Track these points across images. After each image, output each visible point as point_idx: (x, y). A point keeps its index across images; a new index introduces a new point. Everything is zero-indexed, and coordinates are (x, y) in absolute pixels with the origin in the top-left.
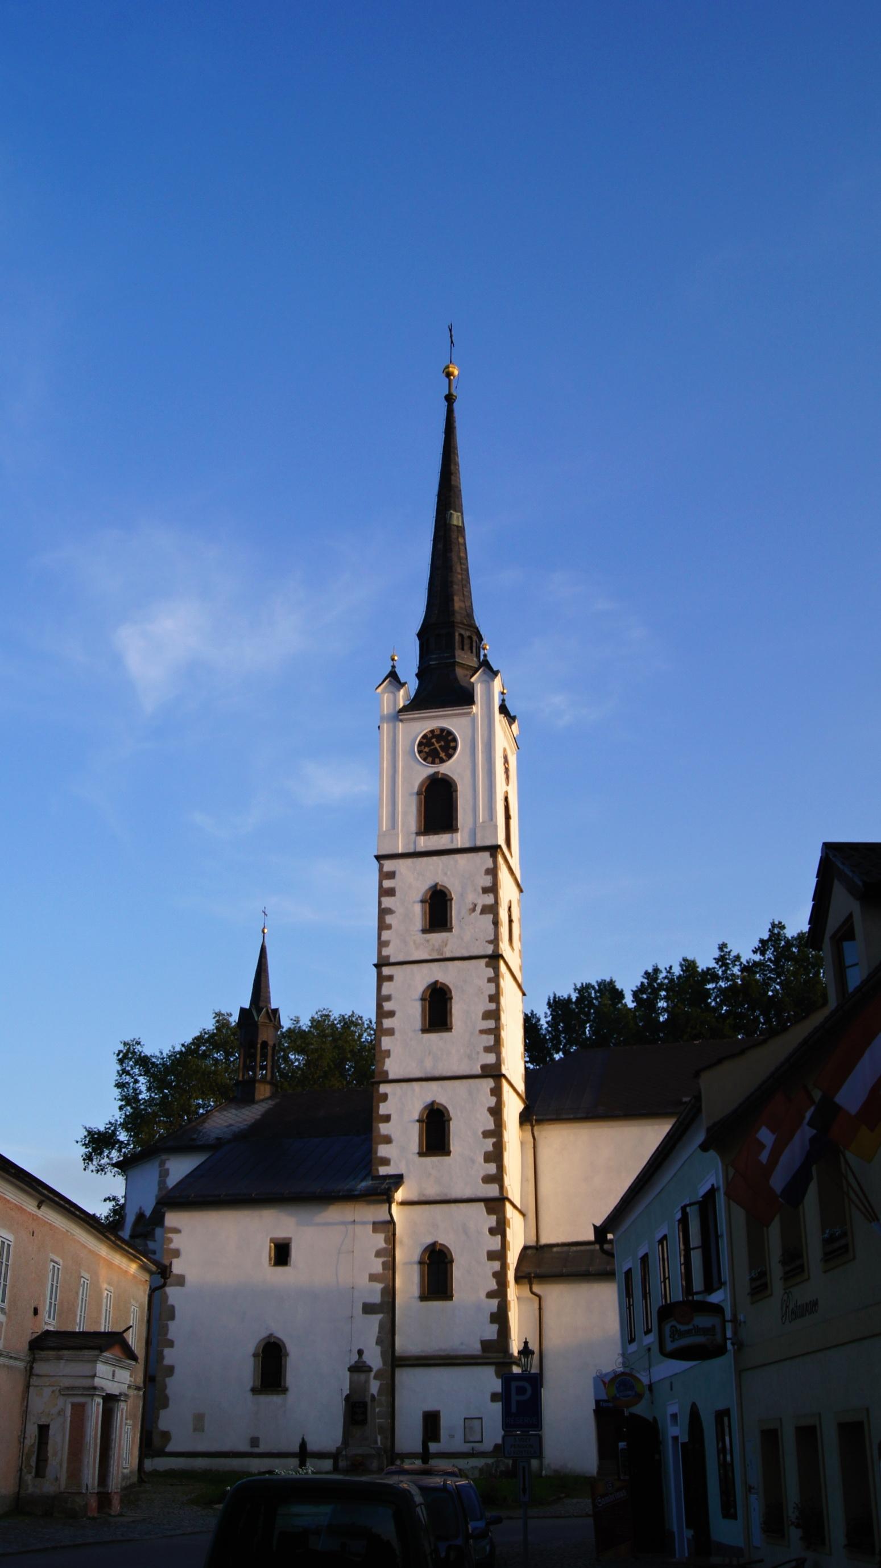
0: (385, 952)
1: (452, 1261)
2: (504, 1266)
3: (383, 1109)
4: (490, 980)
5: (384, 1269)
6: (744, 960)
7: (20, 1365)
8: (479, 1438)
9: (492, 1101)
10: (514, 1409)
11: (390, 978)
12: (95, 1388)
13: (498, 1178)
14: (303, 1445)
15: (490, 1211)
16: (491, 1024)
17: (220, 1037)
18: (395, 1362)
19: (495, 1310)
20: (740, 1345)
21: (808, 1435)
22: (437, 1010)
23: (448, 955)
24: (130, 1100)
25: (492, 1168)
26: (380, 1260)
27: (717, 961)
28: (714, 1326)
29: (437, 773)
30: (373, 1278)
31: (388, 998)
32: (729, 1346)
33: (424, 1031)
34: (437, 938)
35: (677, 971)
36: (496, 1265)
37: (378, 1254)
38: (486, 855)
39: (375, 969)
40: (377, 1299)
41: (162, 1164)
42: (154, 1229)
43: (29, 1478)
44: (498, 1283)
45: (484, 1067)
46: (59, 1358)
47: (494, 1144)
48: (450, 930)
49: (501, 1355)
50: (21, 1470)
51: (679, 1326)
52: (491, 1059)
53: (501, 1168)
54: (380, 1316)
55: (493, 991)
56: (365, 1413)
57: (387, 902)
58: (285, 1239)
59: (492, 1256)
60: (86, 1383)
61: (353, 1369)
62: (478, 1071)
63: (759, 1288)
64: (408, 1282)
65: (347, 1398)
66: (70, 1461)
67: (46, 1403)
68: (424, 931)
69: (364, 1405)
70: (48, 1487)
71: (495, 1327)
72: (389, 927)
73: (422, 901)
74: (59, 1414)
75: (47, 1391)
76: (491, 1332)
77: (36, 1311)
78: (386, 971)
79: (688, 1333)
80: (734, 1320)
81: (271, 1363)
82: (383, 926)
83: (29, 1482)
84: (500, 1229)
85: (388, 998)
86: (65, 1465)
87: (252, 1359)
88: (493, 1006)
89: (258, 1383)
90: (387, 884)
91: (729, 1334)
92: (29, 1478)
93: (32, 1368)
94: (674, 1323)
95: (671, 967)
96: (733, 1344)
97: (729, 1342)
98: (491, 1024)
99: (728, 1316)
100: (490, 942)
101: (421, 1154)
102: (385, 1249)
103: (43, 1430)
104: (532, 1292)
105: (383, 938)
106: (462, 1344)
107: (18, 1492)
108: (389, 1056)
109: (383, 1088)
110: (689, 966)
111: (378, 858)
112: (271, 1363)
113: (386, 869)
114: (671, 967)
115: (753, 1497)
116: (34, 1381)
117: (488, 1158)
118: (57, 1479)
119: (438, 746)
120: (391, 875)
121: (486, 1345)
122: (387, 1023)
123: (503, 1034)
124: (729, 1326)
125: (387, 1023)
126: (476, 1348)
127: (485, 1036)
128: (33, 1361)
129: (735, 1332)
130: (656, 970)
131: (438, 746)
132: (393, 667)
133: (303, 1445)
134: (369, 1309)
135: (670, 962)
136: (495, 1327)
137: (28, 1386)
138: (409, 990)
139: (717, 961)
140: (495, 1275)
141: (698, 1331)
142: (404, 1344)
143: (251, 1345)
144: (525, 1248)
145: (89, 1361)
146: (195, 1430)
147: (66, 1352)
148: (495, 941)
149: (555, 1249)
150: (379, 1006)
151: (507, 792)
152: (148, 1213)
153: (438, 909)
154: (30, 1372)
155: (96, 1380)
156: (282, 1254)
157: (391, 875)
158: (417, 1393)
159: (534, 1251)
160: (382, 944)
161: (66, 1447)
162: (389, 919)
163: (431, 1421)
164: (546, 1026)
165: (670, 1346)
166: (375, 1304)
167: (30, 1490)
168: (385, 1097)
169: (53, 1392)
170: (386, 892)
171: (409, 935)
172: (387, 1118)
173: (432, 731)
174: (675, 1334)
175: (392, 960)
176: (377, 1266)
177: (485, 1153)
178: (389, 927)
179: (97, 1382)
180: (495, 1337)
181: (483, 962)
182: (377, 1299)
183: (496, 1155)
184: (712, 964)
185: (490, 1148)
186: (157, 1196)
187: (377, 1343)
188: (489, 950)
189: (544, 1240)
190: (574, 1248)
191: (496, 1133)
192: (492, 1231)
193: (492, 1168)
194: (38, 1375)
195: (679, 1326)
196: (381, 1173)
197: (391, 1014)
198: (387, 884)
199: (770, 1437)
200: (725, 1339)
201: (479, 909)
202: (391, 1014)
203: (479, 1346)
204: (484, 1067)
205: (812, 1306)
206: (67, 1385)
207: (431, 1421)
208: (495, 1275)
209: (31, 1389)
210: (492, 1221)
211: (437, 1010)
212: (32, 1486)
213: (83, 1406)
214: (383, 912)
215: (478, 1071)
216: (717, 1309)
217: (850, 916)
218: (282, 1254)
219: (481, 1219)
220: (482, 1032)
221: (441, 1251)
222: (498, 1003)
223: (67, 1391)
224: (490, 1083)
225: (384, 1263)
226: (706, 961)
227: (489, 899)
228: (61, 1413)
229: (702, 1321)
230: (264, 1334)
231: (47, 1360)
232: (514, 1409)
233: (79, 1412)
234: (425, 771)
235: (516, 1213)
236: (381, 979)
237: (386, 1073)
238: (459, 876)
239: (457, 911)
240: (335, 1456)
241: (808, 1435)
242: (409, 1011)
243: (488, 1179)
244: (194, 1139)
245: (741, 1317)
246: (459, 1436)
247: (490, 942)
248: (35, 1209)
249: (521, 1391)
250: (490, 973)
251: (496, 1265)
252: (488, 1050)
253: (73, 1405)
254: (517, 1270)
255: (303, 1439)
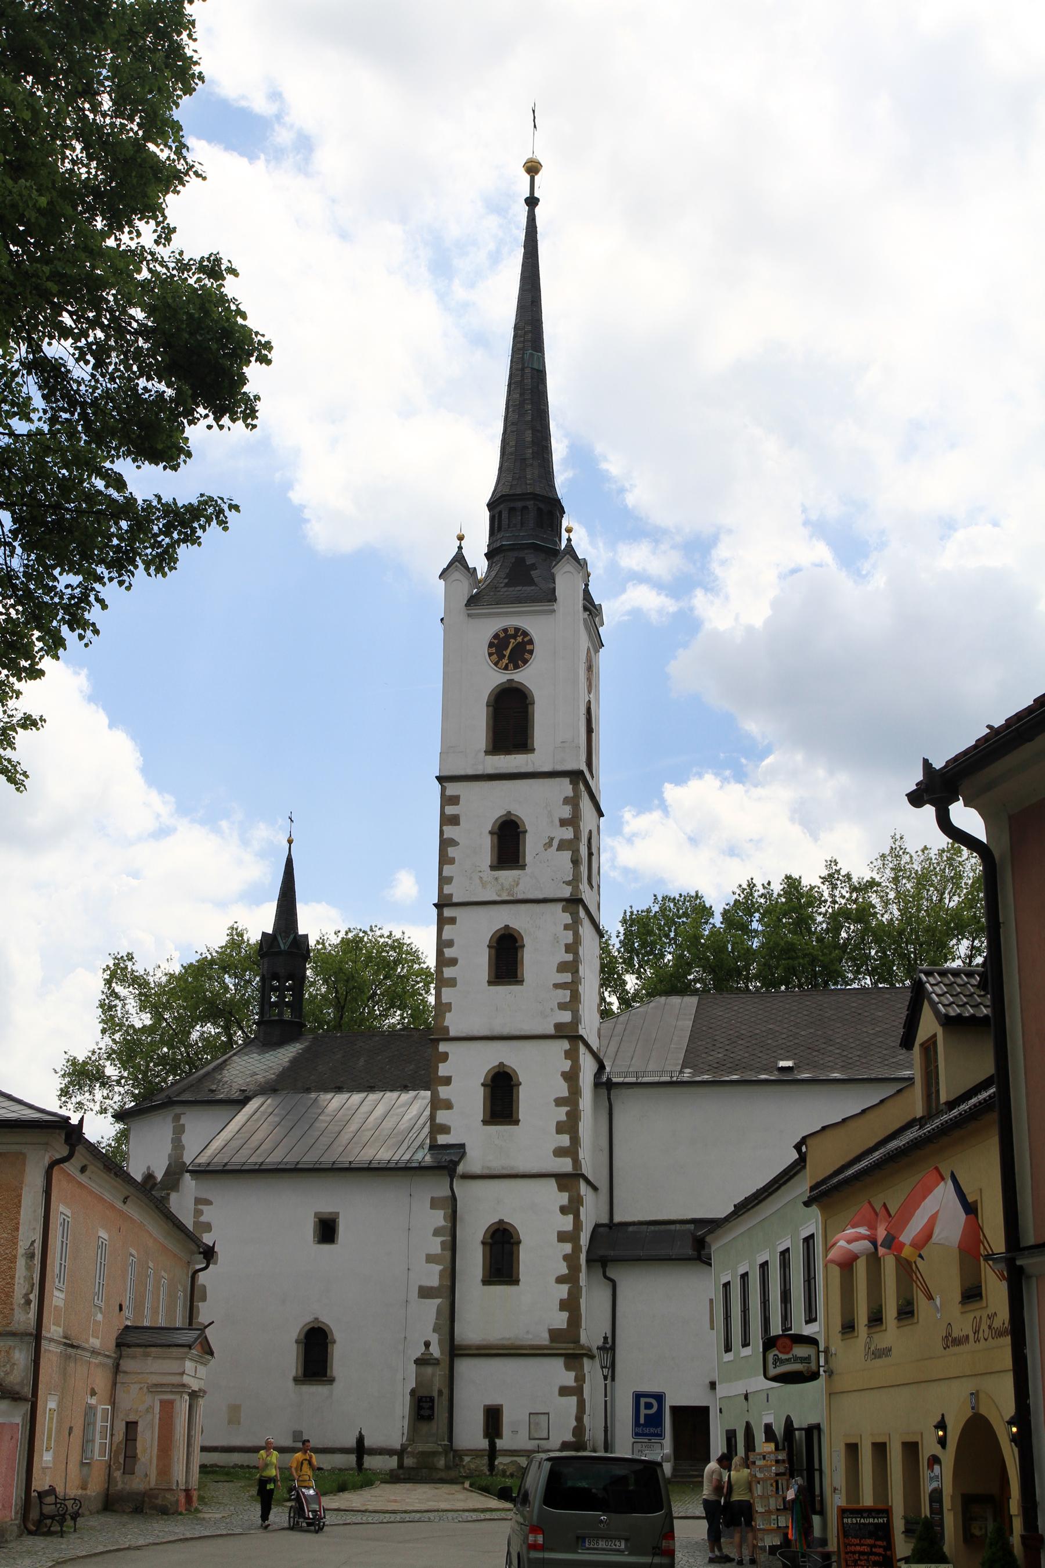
0: (447, 890)
1: (519, 1242)
2: (577, 1248)
3: (443, 1070)
4: (567, 927)
5: (442, 1249)
6: (855, 880)
7: (110, 1361)
8: (545, 1436)
9: (567, 1065)
10: (642, 1421)
11: (452, 921)
12: (184, 1385)
13: (571, 1152)
14: (360, 1440)
15: (561, 1188)
16: (567, 977)
17: (232, 957)
18: (455, 1351)
19: (565, 1296)
20: (830, 1373)
21: (880, 1449)
22: (506, 958)
23: (521, 896)
24: (111, 1022)
25: (565, 1140)
26: (439, 1239)
27: (824, 880)
28: (810, 1356)
29: (510, 681)
30: (430, 1259)
31: (450, 944)
32: (822, 1372)
33: (490, 983)
34: (507, 876)
35: (777, 888)
36: (568, 1248)
37: (437, 1232)
38: (566, 782)
39: (435, 911)
40: (434, 1281)
41: (177, 1118)
42: (168, 1194)
43: (118, 1474)
44: (569, 1267)
45: (558, 1026)
46: (147, 1355)
47: (568, 1114)
48: (523, 867)
49: (572, 1345)
50: (110, 1466)
51: (781, 1356)
52: (566, 1017)
53: (575, 1140)
54: (439, 1301)
55: (570, 940)
56: (432, 1408)
57: (450, 832)
58: (331, 1213)
59: (562, 1237)
60: (175, 1380)
61: (419, 1362)
62: (551, 1031)
63: (848, 1327)
64: (473, 1260)
65: (413, 1392)
66: (159, 1458)
67: (136, 1400)
68: (493, 868)
69: (431, 1399)
70: (137, 1484)
71: (565, 1315)
72: (452, 861)
73: (491, 833)
74: (147, 1411)
75: (134, 1388)
76: (560, 1320)
77: (121, 1309)
78: (448, 912)
79: (788, 1360)
80: (827, 1351)
81: (315, 1352)
82: (444, 859)
83: (118, 1479)
84: (572, 1208)
85: (450, 944)
86: (155, 1461)
87: (295, 1346)
88: (569, 957)
89: (300, 1372)
90: (450, 810)
91: (822, 1363)
92: (118, 1474)
93: (118, 1365)
94: (777, 1352)
95: (769, 883)
96: (825, 1371)
97: (822, 1369)
98: (567, 977)
99: (822, 1348)
100: (568, 883)
101: (485, 1122)
102: (443, 1227)
103: (131, 1427)
104: (605, 1277)
105: (445, 874)
106: (528, 1332)
107: (108, 1489)
108: (450, 1011)
109: (443, 1047)
110: (792, 884)
111: (440, 779)
112: (315, 1352)
113: (448, 793)
114: (769, 883)
115: (837, 1496)
116: (120, 1378)
117: (560, 1128)
118: (146, 1475)
119: (512, 649)
120: (454, 800)
121: (555, 1335)
122: (448, 972)
123: (581, 989)
124: (822, 1355)
125: (448, 972)
126: (544, 1339)
127: (560, 992)
128: (120, 1357)
129: (827, 1362)
130: (751, 885)
131: (512, 649)
132: (460, 548)
133: (360, 1440)
134: (425, 1293)
135: (769, 874)
136: (565, 1315)
137: (114, 1384)
138: (476, 932)
139: (824, 880)
140: (566, 1258)
141: (797, 1359)
142: (468, 1332)
143: (294, 1331)
144: (597, 1226)
145: (176, 1358)
146: (230, 1422)
147: (153, 1349)
148: (575, 882)
149: (631, 1229)
150: (440, 953)
151: (589, 702)
152: (159, 1175)
153: (509, 842)
154: (117, 1369)
155: (185, 1376)
156: (327, 1230)
157: (454, 800)
158: (478, 1385)
159: (607, 1229)
160: (444, 880)
161: (156, 1443)
162: (452, 852)
163: (493, 1417)
164: (618, 945)
165: (773, 1372)
166: (432, 1288)
167: (120, 1486)
168: (445, 1057)
169: (141, 1388)
170: (448, 820)
171: (476, 874)
172: (447, 1081)
173: (505, 630)
174: (777, 1361)
175: (455, 900)
176: (436, 1246)
177: (558, 1123)
178: (452, 861)
179: (186, 1379)
180: (565, 1327)
181: (559, 906)
182: (434, 1281)
183: (570, 1126)
184: (817, 882)
185: (564, 1118)
186: (170, 1156)
187: (434, 1331)
188: (566, 892)
189: (617, 1219)
190: (652, 1228)
191: (571, 1101)
192: (564, 1210)
193: (565, 1140)
194: (125, 1372)
195: (781, 1356)
196: (439, 1142)
197: (453, 962)
198: (450, 810)
199: (852, 1449)
200: (819, 1366)
201: (555, 843)
202: (453, 962)
203: (546, 1335)
204: (558, 1026)
205: (886, 1352)
206: (154, 1382)
207: (493, 1417)
208: (566, 1258)
209: (118, 1385)
210: (564, 1198)
211: (506, 958)
212: (121, 1483)
213: (171, 1403)
214: (445, 844)
215: (551, 1031)
216: (812, 1341)
217: (935, 1035)
218: (327, 1230)
219: (553, 1196)
220: (557, 986)
221: (505, 1230)
222: (576, 954)
223: (155, 1388)
224: (566, 1045)
225: (442, 1243)
226: (811, 878)
227: (568, 833)
228: (149, 1410)
229: (800, 1351)
230: (309, 1318)
231: (134, 1357)
232: (642, 1421)
233: (167, 1407)
234: (498, 678)
235: (590, 1189)
236: (442, 922)
237: (447, 1029)
238: (539, 808)
239: (532, 846)
240: (401, 1453)
241: (880, 1449)
242: (475, 960)
243: (559, 1152)
244: (213, 1091)
245: (833, 1349)
246: (524, 1433)
247: (568, 883)
248: (121, 1204)
249: (649, 1406)
250: (567, 919)
251: (568, 1248)
252: (562, 1006)
253: (161, 1402)
254: (588, 1252)
255: (360, 1432)
